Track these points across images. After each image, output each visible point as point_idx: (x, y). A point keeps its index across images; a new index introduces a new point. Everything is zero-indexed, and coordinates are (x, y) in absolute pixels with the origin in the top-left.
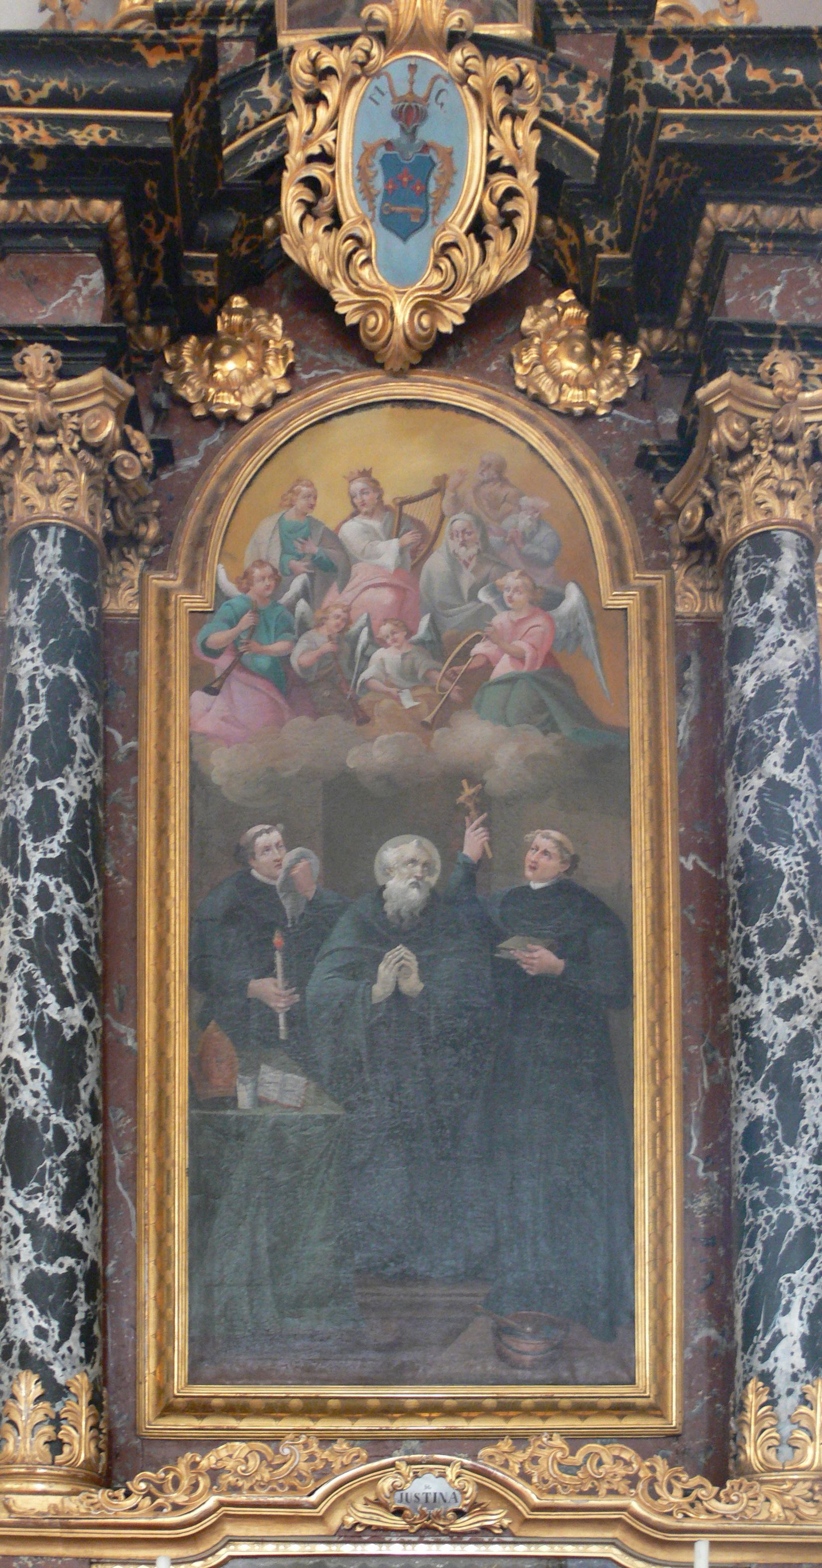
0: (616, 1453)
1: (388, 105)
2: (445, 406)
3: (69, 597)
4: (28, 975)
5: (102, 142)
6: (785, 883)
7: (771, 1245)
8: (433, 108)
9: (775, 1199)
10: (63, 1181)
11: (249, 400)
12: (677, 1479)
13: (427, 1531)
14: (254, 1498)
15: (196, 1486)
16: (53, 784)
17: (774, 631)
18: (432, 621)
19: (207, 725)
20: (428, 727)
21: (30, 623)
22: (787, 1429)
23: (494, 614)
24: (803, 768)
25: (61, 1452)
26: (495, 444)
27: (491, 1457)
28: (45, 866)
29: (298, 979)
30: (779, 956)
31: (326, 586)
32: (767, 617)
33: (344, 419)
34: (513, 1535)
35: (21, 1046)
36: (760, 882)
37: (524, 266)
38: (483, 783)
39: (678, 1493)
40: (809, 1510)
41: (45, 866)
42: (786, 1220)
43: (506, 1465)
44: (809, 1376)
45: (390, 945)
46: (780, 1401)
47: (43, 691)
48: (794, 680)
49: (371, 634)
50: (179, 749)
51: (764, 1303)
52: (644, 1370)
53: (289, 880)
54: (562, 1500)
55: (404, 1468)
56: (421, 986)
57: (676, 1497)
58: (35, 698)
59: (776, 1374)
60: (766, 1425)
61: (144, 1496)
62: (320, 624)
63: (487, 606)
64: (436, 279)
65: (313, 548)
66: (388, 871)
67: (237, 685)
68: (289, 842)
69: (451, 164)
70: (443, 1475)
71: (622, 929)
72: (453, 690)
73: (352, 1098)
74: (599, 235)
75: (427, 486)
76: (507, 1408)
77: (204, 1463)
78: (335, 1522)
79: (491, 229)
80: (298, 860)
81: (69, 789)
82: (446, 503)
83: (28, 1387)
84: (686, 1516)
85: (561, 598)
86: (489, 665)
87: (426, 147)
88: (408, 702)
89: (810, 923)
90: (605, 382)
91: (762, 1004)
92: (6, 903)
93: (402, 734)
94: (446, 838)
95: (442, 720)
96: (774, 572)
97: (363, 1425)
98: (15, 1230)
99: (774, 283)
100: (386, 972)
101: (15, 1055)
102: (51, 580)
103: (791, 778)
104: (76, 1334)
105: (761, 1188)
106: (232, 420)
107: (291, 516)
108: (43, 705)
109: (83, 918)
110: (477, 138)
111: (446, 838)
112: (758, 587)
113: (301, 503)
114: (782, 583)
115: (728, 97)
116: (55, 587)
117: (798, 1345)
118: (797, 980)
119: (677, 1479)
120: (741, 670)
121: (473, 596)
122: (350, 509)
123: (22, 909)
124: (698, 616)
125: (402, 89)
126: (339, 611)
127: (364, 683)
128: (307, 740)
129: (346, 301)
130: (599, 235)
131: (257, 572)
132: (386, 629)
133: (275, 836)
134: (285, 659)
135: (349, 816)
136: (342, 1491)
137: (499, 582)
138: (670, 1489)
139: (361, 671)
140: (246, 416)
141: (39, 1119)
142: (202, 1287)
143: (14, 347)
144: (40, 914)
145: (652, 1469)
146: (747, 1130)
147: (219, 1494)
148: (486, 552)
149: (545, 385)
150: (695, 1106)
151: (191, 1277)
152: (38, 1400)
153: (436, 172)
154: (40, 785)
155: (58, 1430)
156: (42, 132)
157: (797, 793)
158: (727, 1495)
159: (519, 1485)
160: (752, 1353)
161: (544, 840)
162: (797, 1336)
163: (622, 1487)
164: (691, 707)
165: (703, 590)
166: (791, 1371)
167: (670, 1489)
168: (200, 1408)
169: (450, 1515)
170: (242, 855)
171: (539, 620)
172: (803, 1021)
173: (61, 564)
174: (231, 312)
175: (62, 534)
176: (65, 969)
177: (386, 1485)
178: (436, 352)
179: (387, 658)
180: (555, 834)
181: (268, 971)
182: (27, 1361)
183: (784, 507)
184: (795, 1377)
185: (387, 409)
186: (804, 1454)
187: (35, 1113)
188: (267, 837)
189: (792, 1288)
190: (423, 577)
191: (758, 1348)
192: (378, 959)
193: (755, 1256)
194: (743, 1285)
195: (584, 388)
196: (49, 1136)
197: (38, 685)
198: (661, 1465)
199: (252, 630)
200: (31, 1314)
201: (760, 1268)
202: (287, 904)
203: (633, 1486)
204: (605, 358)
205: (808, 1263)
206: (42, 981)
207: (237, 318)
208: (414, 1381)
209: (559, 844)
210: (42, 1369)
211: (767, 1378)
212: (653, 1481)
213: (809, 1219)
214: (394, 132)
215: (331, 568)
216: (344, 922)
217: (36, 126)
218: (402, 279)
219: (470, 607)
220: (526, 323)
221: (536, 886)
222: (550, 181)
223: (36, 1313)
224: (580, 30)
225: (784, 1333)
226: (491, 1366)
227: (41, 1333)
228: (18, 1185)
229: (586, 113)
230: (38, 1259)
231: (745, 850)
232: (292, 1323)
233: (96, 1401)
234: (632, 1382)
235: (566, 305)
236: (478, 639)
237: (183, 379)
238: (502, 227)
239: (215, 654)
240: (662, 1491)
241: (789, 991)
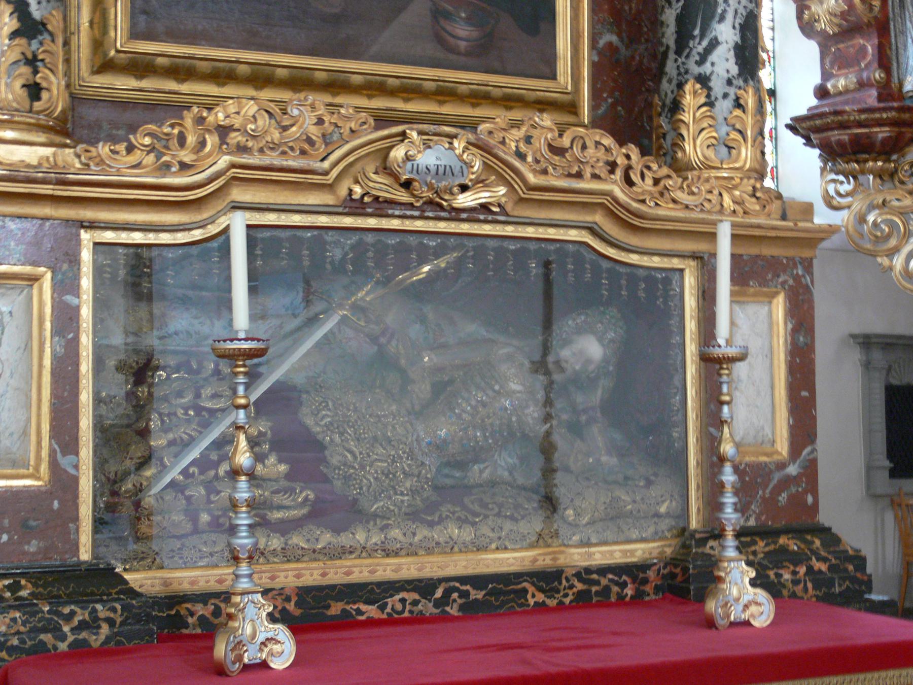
0: (597, 139)
12: (649, 168)
13: (435, 206)
14: (266, 160)
15: (203, 144)
25: (39, 99)
27: (490, 133)
34: (507, 215)
39: (649, 181)
44: (741, 82)
46: (717, 104)
59: (713, 78)
60: (705, 125)
61: (149, 153)
70: (452, 148)
76: (445, 93)
77: (211, 119)
84: (657, 204)
117: (732, 53)
119: (649, 168)
136: (351, 159)
138: (643, 176)
145: (628, 157)
147: (229, 154)
152: (14, 35)
155: (36, 72)
158: (688, 186)
159: (517, 164)
160: (687, 57)
162: (731, 44)
163: (603, 172)
166: (726, 76)
167: (643, 176)
168: (140, 67)
169: (456, 190)
186: (739, 153)
191: (694, 52)
203: (612, 172)
208: (357, 57)
211: (704, 80)
212: (629, 168)
225: (720, 39)
226: (431, 49)
234: (553, 77)
240: (635, 178)
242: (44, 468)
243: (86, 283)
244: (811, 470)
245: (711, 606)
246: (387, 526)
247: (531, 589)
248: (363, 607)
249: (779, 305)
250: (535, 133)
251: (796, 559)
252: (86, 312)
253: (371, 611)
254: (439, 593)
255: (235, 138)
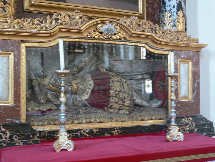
119: (160, 30)
240: (157, 32)
245: (168, 137)
249: (12, 57)
255: (60, 21)
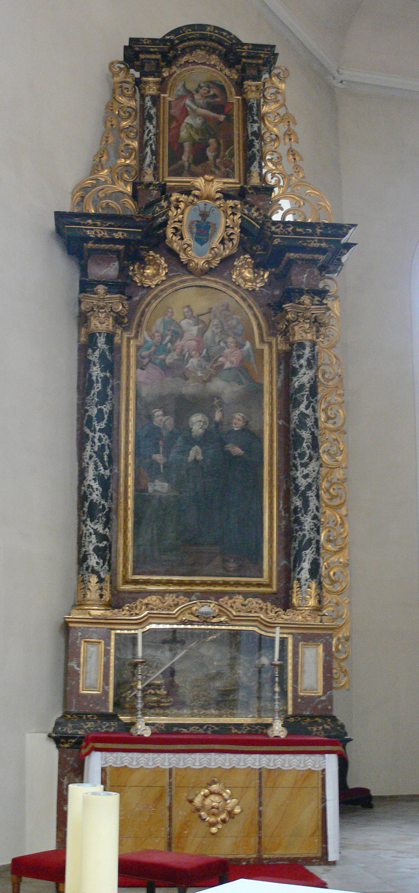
1: (198, 212)
2: (211, 288)
3: (107, 353)
4: (95, 461)
5: (122, 237)
6: (305, 441)
7: (300, 542)
8: (211, 214)
9: (302, 530)
10: (104, 519)
11: (155, 283)
13: (205, 622)
15: (141, 608)
16: (102, 407)
17: (303, 370)
18: (207, 350)
19: (141, 379)
20: (205, 382)
21: (96, 360)
22: (304, 595)
23: (225, 349)
24: (310, 409)
26: (226, 300)
28: (101, 430)
29: (167, 454)
30: (303, 461)
31: (177, 339)
32: (301, 366)
33: (182, 290)
35: (93, 481)
36: (299, 440)
37: (236, 251)
38: (221, 398)
40: (309, 619)
41: (101, 430)
42: (304, 535)
43: (226, 604)
44: (310, 580)
45: (193, 445)
47: (100, 380)
48: (309, 384)
49: (189, 354)
50: (132, 385)
51: (298, 559)
52: (266, 574)
53: (164, 426)
54: (242, 614)
55: (199, 604)
56: (202, 458)
57: (273, 614)
58: (97, 382)
62: (174, 350)
63: (223, 347)
64: (211, 255)
65: (172, 328)
66: (193, 424)
67: (150, 367)
68: (165, 414)
69: (215, 228)
70: (209, 606)
71: (261, 441)
72: (213, 371)
73: (182, 490)
74: (257, 248)
75: (207, 311)
78: (179, 619)
79: (226, 242)
80: (166, 420)
81: (106, 408)
82: (212, 316)
83: (94, 579)
85: (244, 345)
86: (222, 365)
87: (208, 223)
88: (200, 374)
89: (312, 452)
90: (258, 281)
91: (298, 474)
92: (89, 440)
93: (197, 384)
94: (209, 414)
95: (209, 380)
96: (304, 354)
97: (183, 588)
98: (91, 534)
99: (304, 274)
100: (192, 454)
101: (91, 484)
102: (102, 348)
103: (307, 412)
104: (107, 563)
105: (298, 526)
106: (149, 287)
107: (166, 318)
108: (100, 384)
109: (110, 444)
110: (223, 220)
111: (209, 414)
112: (299, 357)
113: (169, 314)
114: (306, 357)
115: (291, 234)
116: (103, 350)
118: (308, 469)
120: (295, 379)
121: (219, 344)
122: (183, 317)
123: (93, 442)
124: (284, 350)
125: (202, 209)
126: (180, 347)
127: (187, 368)
128: (172, 385)
129: (184, 258)
130: (257, 248)
131: (156, 334)
132: (193, 353)
133: (160, 413)
134: (164, 360)
135: (183, 406)
137: (227, 340)
138: (272, 611)
139: (186, 365)
140: (153, 286)
141: (98, 502)
142: (136, 546)
143: (96, 285)
144: (99, 444)
145: (267, 606)
146: (294, 508)
148: (223, 331)
149: (241, 281)
150: (282, 494)
151: (134, 543)
152: (97, 583)
153: (211, 229)
154: (99, 407)
156: (106, 234)
157: (309, 416)
159: (230, 609)
161: (238, 416)
162: (307, 569)
163: (258, 610)
164: (282, 376)
165: (286, 343)
167: (272, 611)
168: (136, 582)
170: (150, 417)
171: (238, 351)
172: (309, 480)
173: (105, 343)
174: (150, 256)
175: (105, 335)
176: (106, 459)
177: (194, 608)
178: (210, 271)
179: (193, 362)
180: (242, 414)
181: (158, 452)
182: (94, 572)
183: (306, 335)
184: (306, 580)
185: (195, 288)
187: (97, 501)
188: (158, 413)
189: (306, 555)
190: (205, 338)
192: (190, 450)
193: (296, 545)
194: (293, 552)
195: (252, 283)
196: (101, 507)
197: (99, 378)
198: (269, 605)
199: (154, 352)
200: (95, 558)
201: (297, 548)
202: (164, 433)
204: (258, 274)
205: (310, 549)
206: (100, 463)
207: (151, 258)
208: (199, 575)
209: (243, 417)
210: (97, 573)
211: (299, 580)
212: (267, 609)
213: (311, 536)
214: (200, 219)
215: (178, 334)
216: (180, 438)
217: (104, 232)
218: (200, 254)
219: (218, 347)
220: (235, 263)
221: (236, 429)
222: (244, 229)
223: (96, 557)
224: (252, 193)
226: (221, 571)
227: (98, 563)
228: (92, 521)
229: (254, 215)
230: (97, 542)
231: (294, 430)
232: (163, 557)
233: (111, 583)
234: (262, 577)
235: (247, 258)
236: (220, 356)
237: (135, 275)
238: (229, 241)
239: (144, 358)
240: (269, 612)
241: (306, 471)
242: (101, 689)
243: (113, 644)
244: (330, 700)
246: (193, 709)
247: (233, 728)
248: (183, 730)
249: (321, 648)
250: (237, 600)
251: (319, 724)
252: (112, 651)
253: (185, 731)
254: (205, 727)
255: (150, 606)
